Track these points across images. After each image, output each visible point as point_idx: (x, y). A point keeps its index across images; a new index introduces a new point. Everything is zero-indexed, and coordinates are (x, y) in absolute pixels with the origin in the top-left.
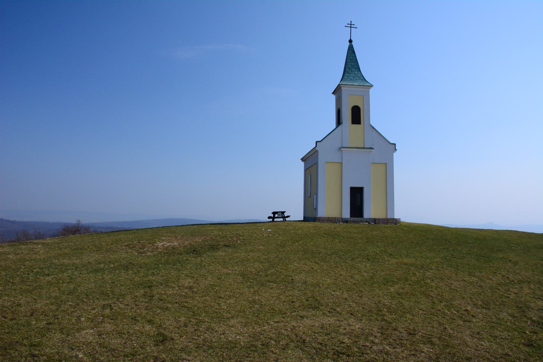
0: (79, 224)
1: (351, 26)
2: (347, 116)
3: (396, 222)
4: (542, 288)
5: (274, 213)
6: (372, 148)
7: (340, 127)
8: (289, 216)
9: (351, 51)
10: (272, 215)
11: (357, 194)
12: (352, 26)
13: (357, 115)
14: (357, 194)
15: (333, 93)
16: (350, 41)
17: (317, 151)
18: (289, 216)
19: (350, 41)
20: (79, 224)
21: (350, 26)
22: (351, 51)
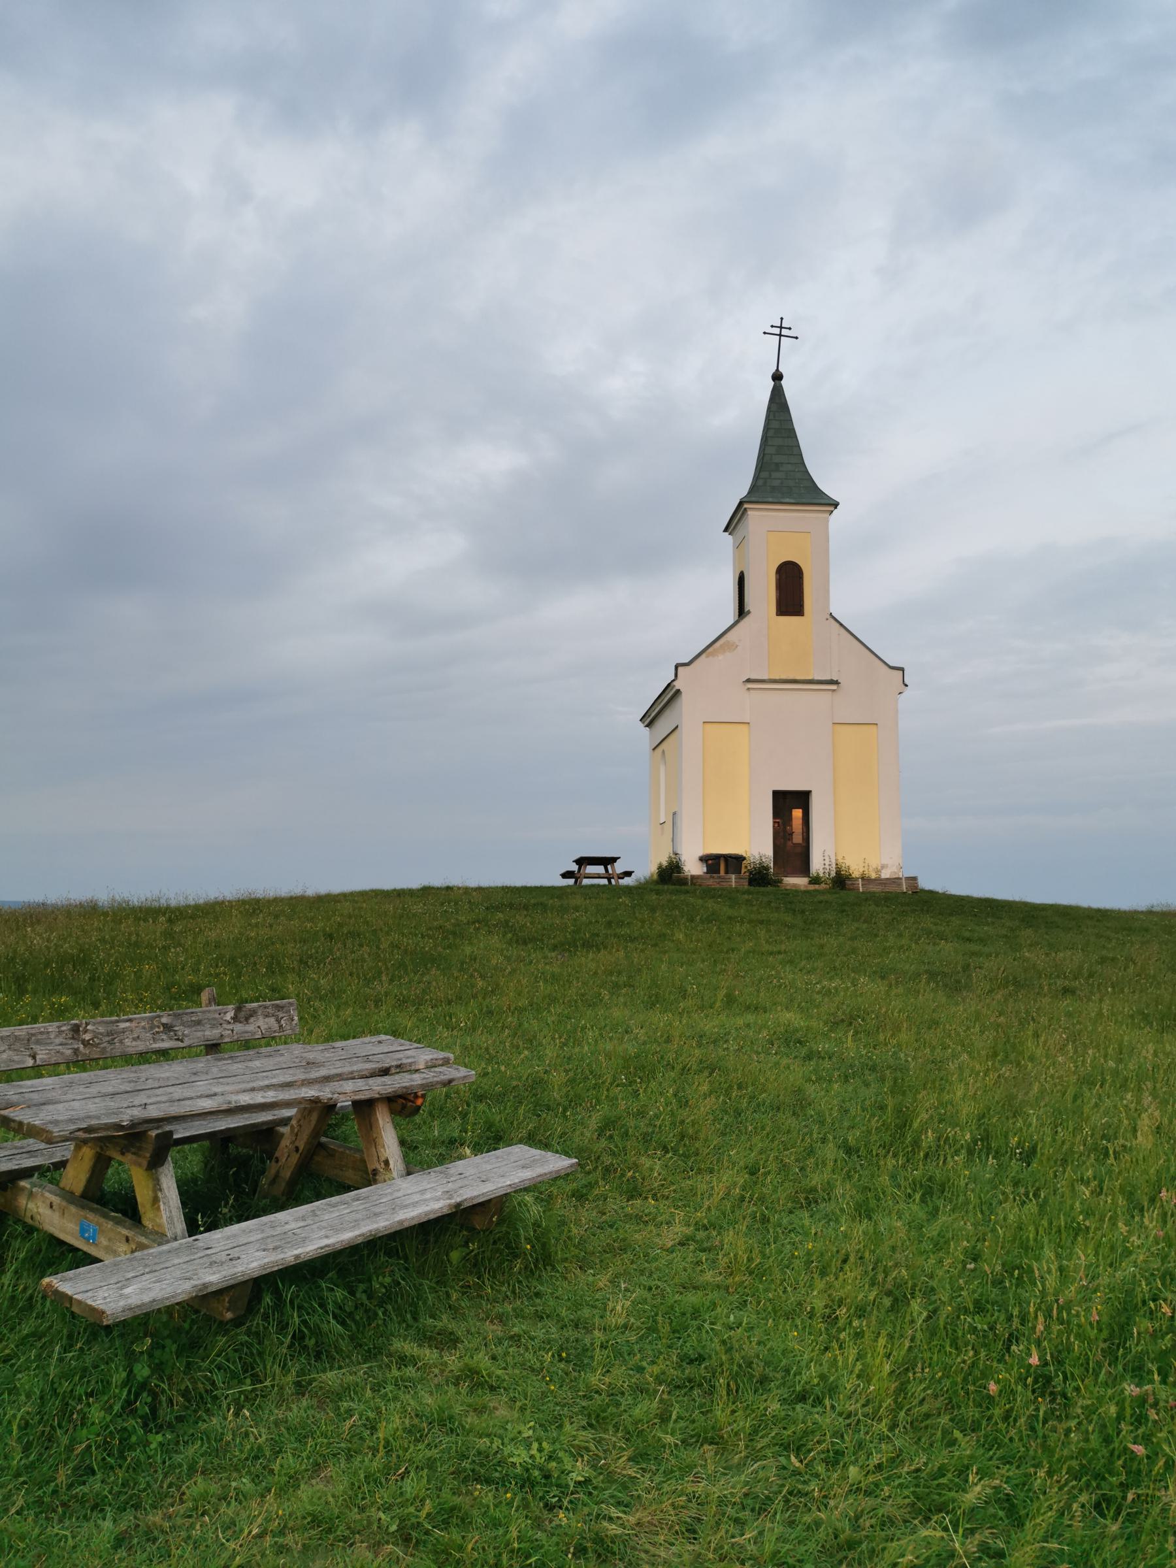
0: (113, 899)
1: (781, 331)
2: (763, 593)
3: (923, 891)
4: (1023, 1556)
5: (582, 862)
6: (837, 683)
7: (746, 621)
8: (628, 874)
9: (778, 403)
10: (575, 868)
11: (790, 804)
12: (784, 332)
13: (790, 589)
14: (790, 804)
15: (726, 530)
16: (777, 377)
17: (678, 691)
18: (628, 874)
19: (777, 377)
20: (113, 899)
21: (777, 331)
22: (778, 403)
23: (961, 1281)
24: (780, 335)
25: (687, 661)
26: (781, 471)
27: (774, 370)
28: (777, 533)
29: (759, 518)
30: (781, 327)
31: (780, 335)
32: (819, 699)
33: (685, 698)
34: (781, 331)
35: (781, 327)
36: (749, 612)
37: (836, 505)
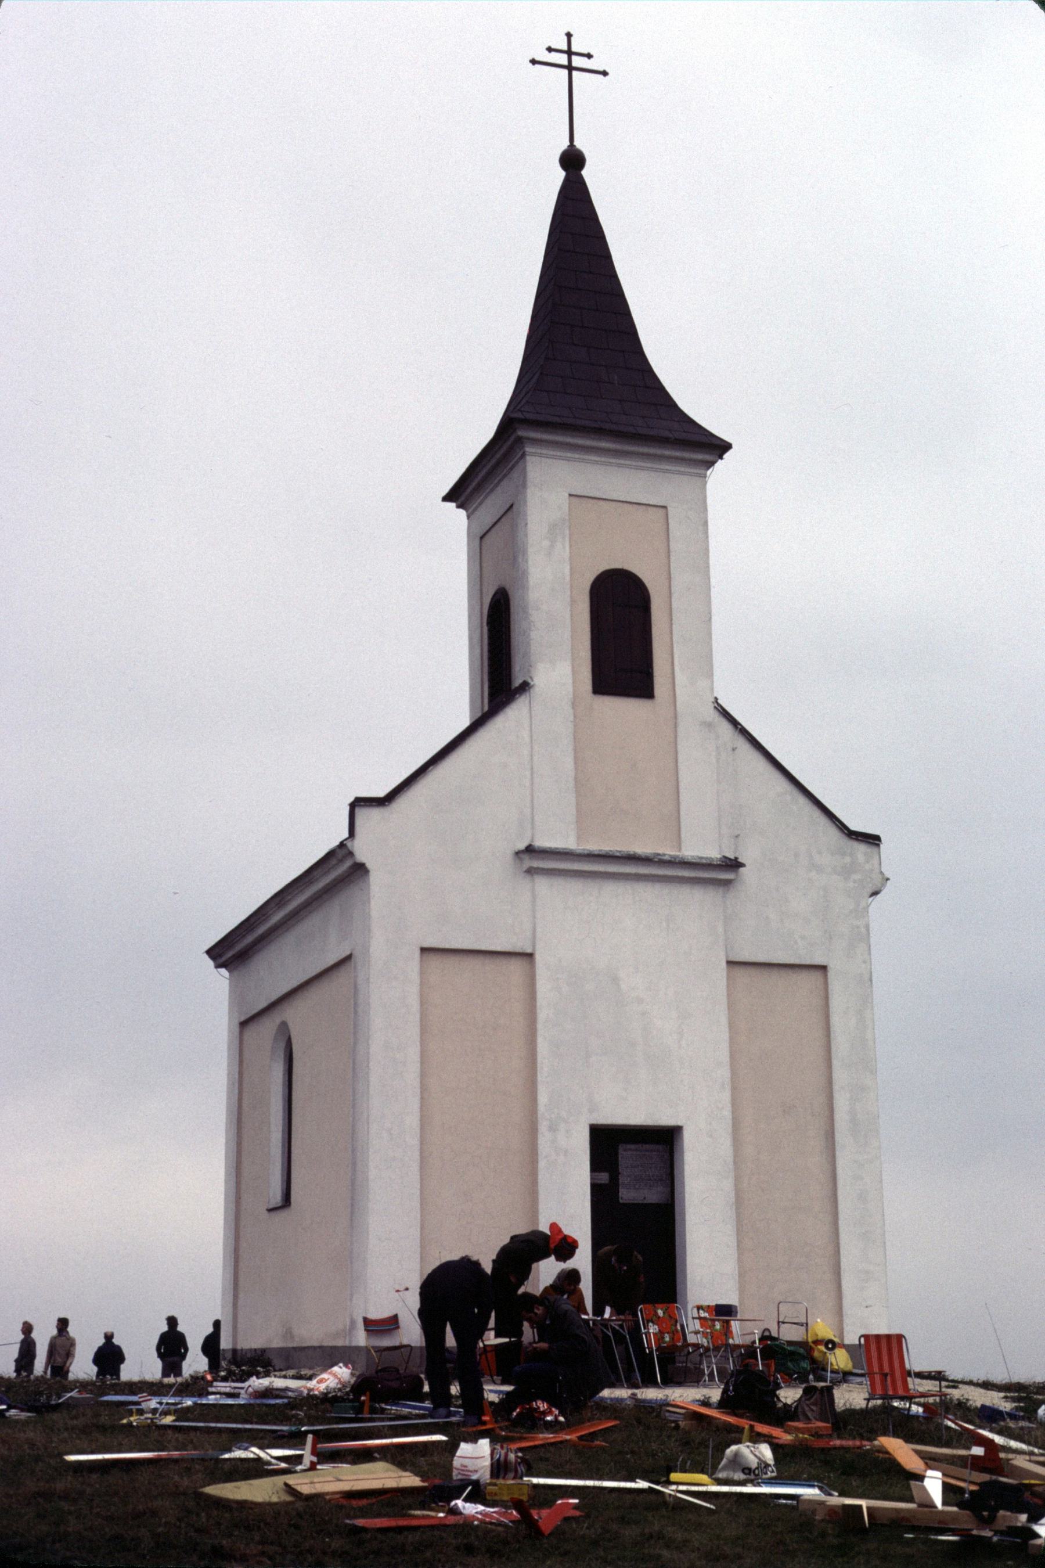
7: (514, 716)
12: (577, 61)
16: (572, 160)
19: (572, 160)
23: (491, 1339)
24: (570, 68)
25: (381, 793)
26: (586, 369)
27: (565, 144)
28: (577, 512)
29: (554, 484)
30: (569, 53)
31: (570, 68)
32: (692, 907)
33: (377, 879)
34: (570, 60)
35: (569, 53)
36: (525, 687)
37: (720, 448)
